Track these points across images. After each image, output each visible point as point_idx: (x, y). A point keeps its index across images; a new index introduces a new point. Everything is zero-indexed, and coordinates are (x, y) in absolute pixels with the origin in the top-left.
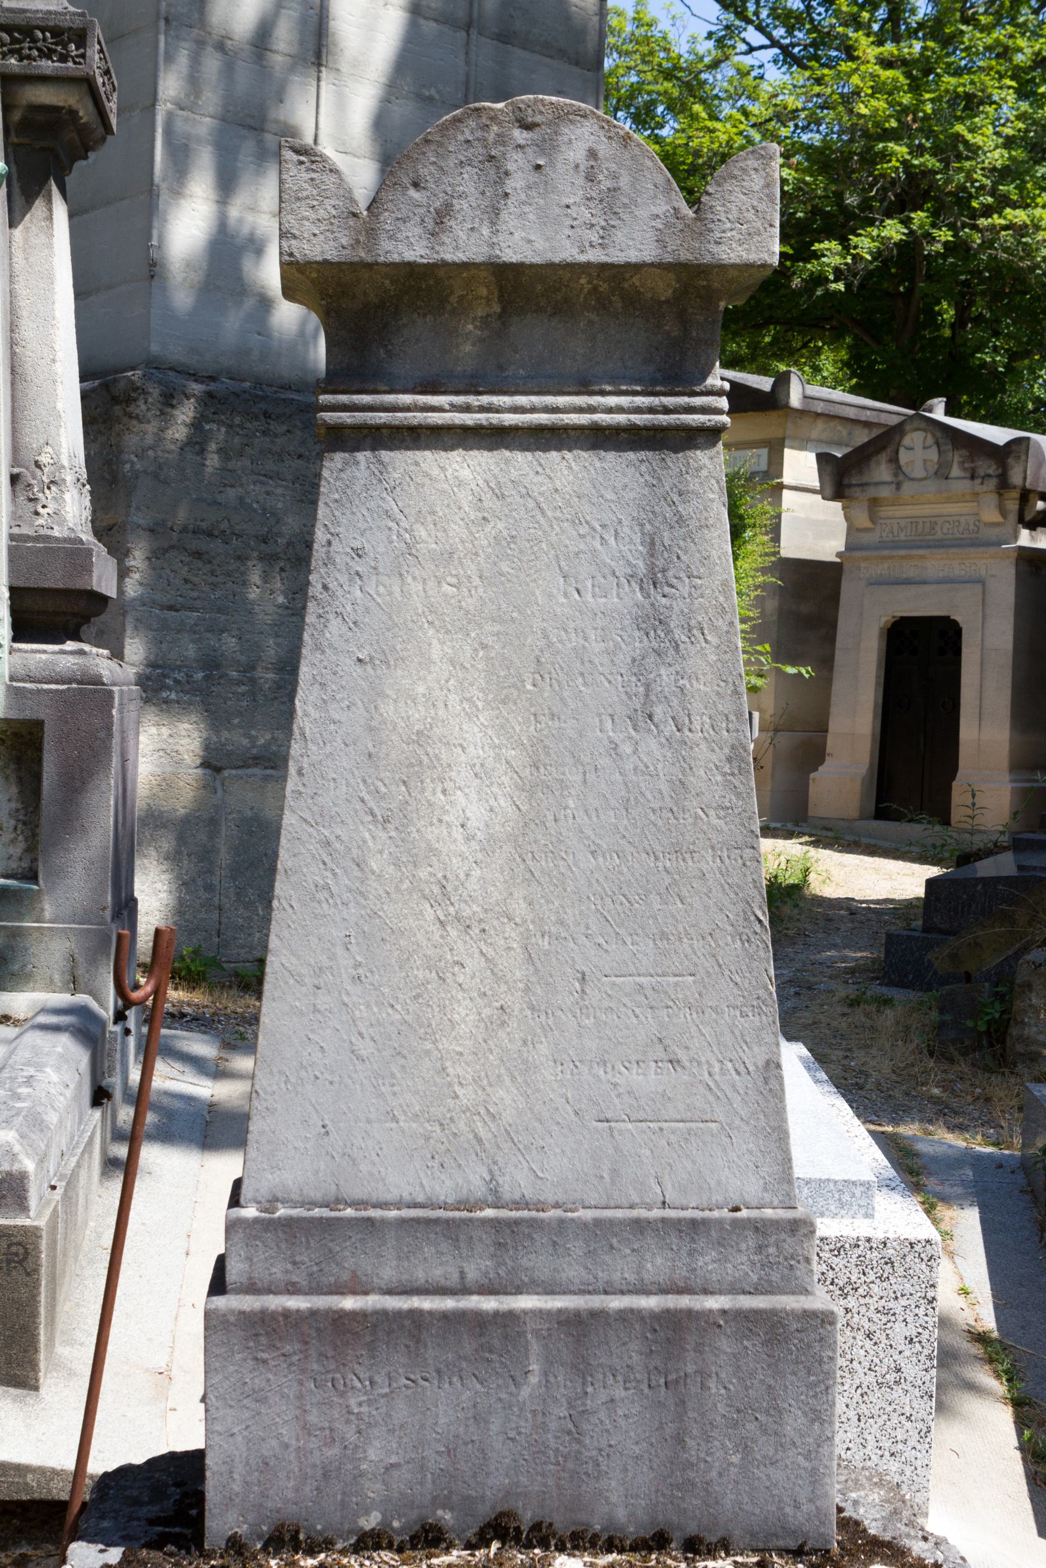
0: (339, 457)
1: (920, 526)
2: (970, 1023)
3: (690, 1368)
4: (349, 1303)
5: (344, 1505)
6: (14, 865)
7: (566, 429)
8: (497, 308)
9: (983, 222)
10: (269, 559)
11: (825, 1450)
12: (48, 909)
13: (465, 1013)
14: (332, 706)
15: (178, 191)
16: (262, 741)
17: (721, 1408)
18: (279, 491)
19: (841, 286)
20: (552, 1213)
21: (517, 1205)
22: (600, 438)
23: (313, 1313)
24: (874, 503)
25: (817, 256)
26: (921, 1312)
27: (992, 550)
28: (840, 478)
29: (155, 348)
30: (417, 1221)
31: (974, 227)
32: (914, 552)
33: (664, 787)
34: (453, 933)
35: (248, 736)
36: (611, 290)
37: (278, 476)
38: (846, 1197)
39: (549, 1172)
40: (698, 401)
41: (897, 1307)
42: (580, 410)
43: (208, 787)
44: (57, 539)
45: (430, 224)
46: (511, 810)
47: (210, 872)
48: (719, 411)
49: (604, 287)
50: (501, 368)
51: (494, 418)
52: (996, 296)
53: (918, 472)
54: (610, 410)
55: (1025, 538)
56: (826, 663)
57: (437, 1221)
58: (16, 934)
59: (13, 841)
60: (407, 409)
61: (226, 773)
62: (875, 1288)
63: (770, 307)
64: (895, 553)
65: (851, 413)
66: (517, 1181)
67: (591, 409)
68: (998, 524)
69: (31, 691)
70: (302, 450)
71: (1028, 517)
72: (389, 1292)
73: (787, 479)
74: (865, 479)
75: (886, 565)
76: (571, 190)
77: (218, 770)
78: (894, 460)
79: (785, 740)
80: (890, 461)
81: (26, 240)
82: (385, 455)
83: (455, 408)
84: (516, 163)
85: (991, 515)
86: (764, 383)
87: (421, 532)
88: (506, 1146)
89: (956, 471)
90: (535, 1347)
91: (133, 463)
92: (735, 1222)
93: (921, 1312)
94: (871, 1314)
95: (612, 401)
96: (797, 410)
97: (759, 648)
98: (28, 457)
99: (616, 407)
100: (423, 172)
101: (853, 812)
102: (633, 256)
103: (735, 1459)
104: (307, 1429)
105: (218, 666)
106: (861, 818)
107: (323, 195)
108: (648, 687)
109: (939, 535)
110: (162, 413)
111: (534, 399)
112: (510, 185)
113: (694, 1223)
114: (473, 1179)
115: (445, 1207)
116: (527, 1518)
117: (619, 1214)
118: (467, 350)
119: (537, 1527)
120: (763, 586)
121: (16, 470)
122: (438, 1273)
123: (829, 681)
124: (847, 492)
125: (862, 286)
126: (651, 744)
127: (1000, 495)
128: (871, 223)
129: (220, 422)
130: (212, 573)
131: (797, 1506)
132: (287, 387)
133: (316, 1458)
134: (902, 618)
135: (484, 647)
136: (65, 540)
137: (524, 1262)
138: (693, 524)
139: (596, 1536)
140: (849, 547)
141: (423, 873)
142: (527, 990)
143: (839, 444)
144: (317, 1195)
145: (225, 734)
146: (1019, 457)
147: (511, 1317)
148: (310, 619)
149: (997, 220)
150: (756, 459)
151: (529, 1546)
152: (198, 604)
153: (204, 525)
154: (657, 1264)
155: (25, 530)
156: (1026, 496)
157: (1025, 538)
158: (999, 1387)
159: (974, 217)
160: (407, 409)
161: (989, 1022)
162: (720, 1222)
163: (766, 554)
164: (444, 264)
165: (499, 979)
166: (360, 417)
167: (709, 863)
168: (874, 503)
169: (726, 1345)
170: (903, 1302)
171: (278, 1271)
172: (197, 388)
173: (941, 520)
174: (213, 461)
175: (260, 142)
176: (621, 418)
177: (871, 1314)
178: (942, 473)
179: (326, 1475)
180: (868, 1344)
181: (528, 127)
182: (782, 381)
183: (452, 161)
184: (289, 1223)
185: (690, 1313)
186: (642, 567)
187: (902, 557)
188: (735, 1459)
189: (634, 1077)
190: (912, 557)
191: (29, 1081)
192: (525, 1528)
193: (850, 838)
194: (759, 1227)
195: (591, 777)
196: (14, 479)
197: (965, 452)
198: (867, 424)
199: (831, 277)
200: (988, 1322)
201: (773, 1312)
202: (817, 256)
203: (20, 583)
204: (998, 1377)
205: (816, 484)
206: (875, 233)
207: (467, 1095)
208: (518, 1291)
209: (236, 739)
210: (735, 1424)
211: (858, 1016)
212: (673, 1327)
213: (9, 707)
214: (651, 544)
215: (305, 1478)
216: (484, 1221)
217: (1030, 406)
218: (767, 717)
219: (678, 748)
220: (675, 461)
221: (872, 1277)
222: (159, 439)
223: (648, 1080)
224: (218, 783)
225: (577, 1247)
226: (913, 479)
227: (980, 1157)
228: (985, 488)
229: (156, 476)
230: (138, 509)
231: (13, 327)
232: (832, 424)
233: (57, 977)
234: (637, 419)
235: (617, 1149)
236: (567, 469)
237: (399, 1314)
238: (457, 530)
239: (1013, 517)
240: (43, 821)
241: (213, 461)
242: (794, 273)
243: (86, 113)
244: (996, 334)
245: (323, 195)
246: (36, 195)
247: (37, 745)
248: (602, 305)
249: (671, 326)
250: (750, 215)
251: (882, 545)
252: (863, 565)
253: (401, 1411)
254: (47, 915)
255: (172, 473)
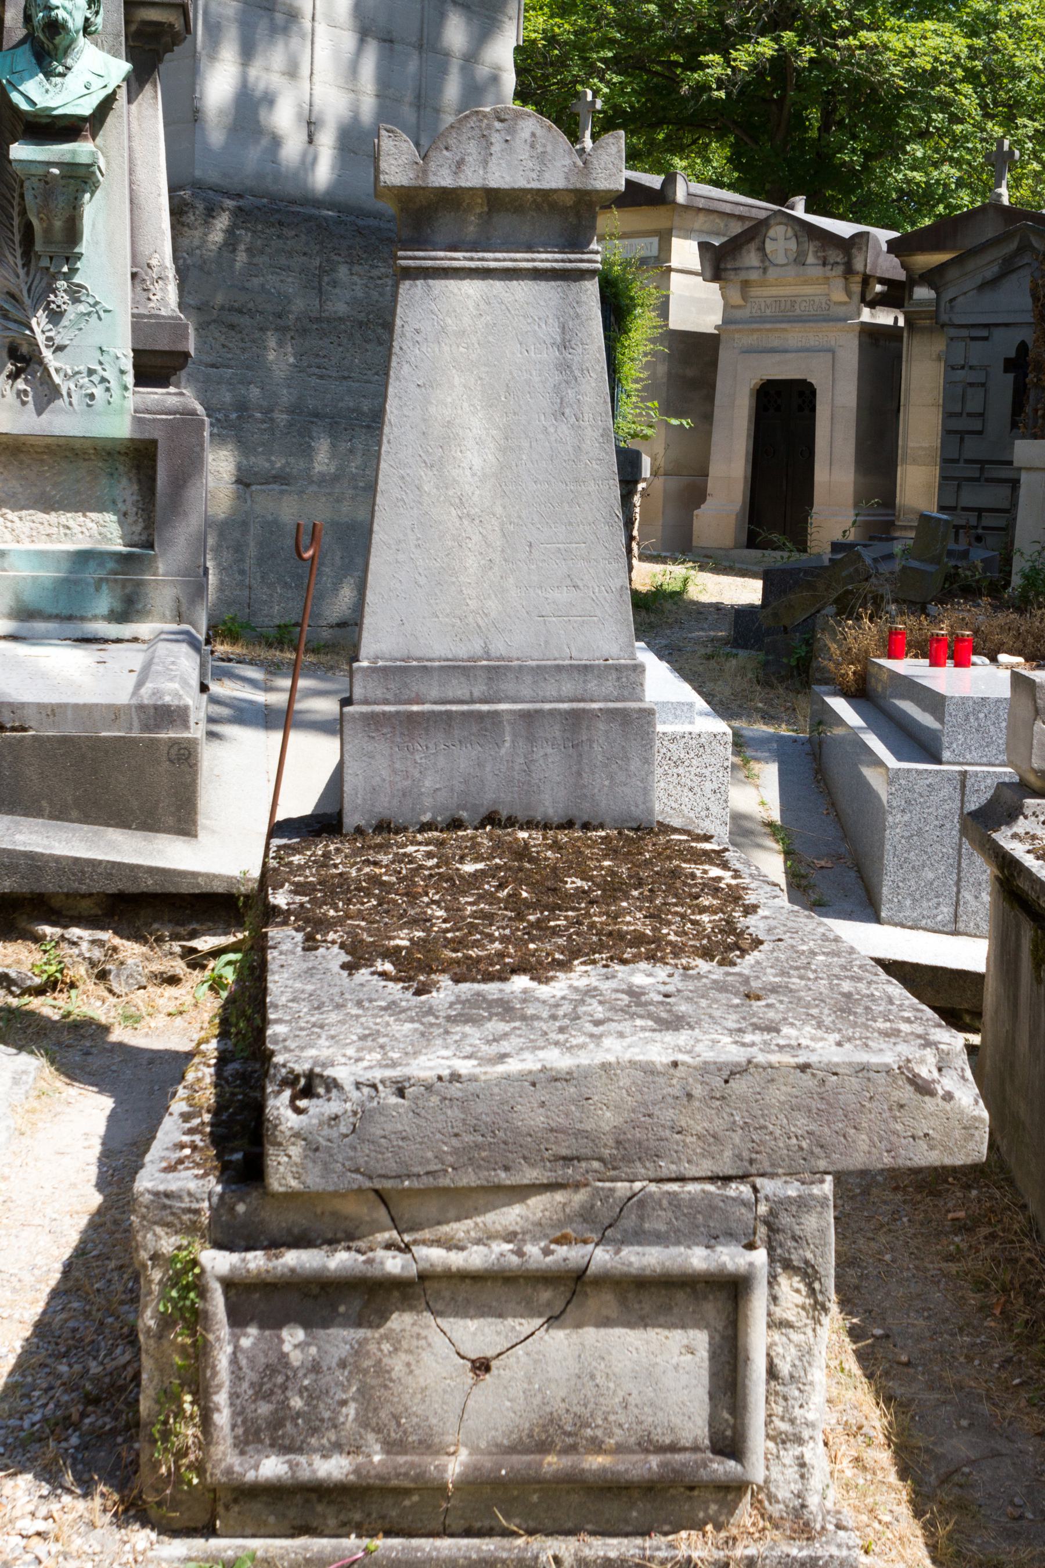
0: (408, 283)
1: (783, 305)
2: (785, 660)
3: (584, 738)
4: (415, 708)
5: (413, 810)
6: (136, 538)
7: (521, 270)
8: (486, 209)
9: (841, 42)
10: (282, 330)
11: (650, 778)
12: (161, 567)
13: (472, 562)
14: (405, 409)
15: (213, 57)
16: (278, 465)
17: (600, 757)
18: (290, 280)
19: (722, 94)
20: (516, 663)
21: (498, 659)
22: (538, 274)
23: (398, 713)
24: (746, 284)
25: (703, 66)
26: (720, 775)
27: (840, 325)
28: (718, 263)
29: (198, 173)
30: (449, 667)
31: (836, 47)
32: (778, 326)
33: (570, 449)
34: (466, 523)
35: (270, 461)
36: (543, 201)
37: (288, 269)
38: (679, 712)
39: (514, 643)
40: (586, 257)
41: (706, 772)
42: (528, 260)
43: (239, 497)
44: (163, 317)
45: (454, 168)
46: (494, 460)
47: (242, 560)
48: (596, 262)
49: (539, 199)
50: (488, 239)
51: (485, 264)
52: (854, 106)
53: (781, 259)
54: (542, 261)
55: (867, 315)
56: (706, 418)
57: (458, 667)
58: (140, 584)
59: (135, 522)
60: (442, 259)
61: (254, 488)
62: (694, 762)
63: (664, 108)
64: (762, 326)
65: (728, 208)
66: (499, 647)
67: (533, 260)
68: (845, 303)
69: (149, 420)
70: (306, 249)
71: (869, 298)
72: (435, 703)
73: (674, 263)
74: (738, 264)
75: (755, 337)
76: (523, 152)
77: (248, 485)
78: (762, 249)
79: (674, 483)
80: (758, 249)
81: (140, 112)
82: (431, 282)
83: (465, 259)
84: (496, 138)
85: (839, 296)
86: (654, 181)
87: (449, 321)
88: (493, 630)
89: (811, 259)
90: (508, 728)
91: (185, 259)
92: (606, 666)
93: (720, 775)
94: (692, 777)
95: (544, 256)
96: (682, 206)
97: (649, 404)
98: (143, 261)
99: (546, 259)
100: (450, 142)
101: (728, 541)
102: (553, 185)
103: (607, 783)
104: (395, 772)
105: (246, 409)
106: (736, 547)
107: (401, 153)
108: (562, 399)
109: (798, 312)
110: (206, 222)
111: (505, 255)
112: (493, 149)
113: (586, 666)
114: (476, 647)
115: (462, 660)
116: (504, 814)
117: (549, 663)
118: (471, 230)
119: (509, 818)
120: (654, 353)
121: (135, 270)
122: (462, 692)
123: (709, 434)
124: (723, 274)
125: (741, 92)
126: (564, 428)
127: (846, 279)
128: (749, 40)
129: (247, 229)
130: (242, 340)
131: (637, 806)
132: (293, 202)
133: (399, 786)
134: (769, 381)
135: (480, 379)
136: (170, 318)
137: (502, 687)
138: (584, 318)
139: (538, 823)
140: (725, 321)
141: (450, 493)
142: (503, 551)
143: (718, 234)
144: (398, 655)
145: (253, 459)
146: (860, 249)
147: (496, 713)
148: (393, 364)
149: (852, 41)
150: (647, 247)
151: (506, 827)
152: (233, 363)
153: (236, 305)
154: (568, 688)
155: (142, 311)
156: (866, 280)
157: (867, 315)
158: (778, 847)
159: (834, 38)
160: (442, 259)
161: (798, 659)
162: (599, 666)
163: (655, 327)
164: (461, 188)
165: (489, 546)
166: (418, 263)
167: (592, 487)
168: (746, 284)
169: (602, 726)
170: (710, 769)
171: (379, 693)
172: (230, 203)
173: (799, 299)
174: (242, 257)
175: (272, 19)
176: (548, 265)
177: (692, 777)
178: (799, 260)
179: (404, 795)
180: (690, 794)
181: (502, 121)
182: (670, 180)
183: (464, 137)
184: (385, 669)
185: (584, 710)
186: (559, 340)
187: (768, 330)
188: (607, 783)
189: (556, 595)
190: (776, 330)
191: (173, 663)
192: (503, 819)
193: (727, 564)
194: (618, 668)
195: (534, 444)
196: (134, 276)
197: (818, 243)
198: (741, 218)
199: (714, 86)
200: (776, 816)
201: (625, 709)
202: (703, 66)
203: (140, 347)
204: (777, 842)
205: (698, 267)
206: (751, 49)
207: (473, 604)
208: (499, 702)
209: (260, 463)
210: (606, 766)
211: (713, 663)
212: (575, 719)
213: (133, 431)
214: (563, 328)
215: (393, 796)
216: (482, 667)
217: (894, 196)
218: (661, 461)
219: (577, 428)
220: (575, 286)
221: (692, 755)
222: (204, 241)
223: (563, 596)
224: (248, 496)
225: (528, 679)
226: (777, 265)
227: (783, 737)
228: (834, 273)
229: (201, 268)
230: (189, 293)
231: (131, 172)
232: (712, 217)
233: (168, 613)
234: (556, 265)
235: (548, 631)
236: (521, 289)
237: (441, 713)
238: (467, 320)
239: (857, 298)
240: (158, 508)
241: (242, 257)
242: (683, 80)
243: (179, 25)
244: (854, 137)
245: (401, 153)
246: (146, 81)
247: (153, 458)
248: (538, 208)
249: (572, 219)
250: (611, 166)
251: (753, 320)
252: (737, 336)
253: (442, 762)
254: (161, 571)
255: (214, 266)
